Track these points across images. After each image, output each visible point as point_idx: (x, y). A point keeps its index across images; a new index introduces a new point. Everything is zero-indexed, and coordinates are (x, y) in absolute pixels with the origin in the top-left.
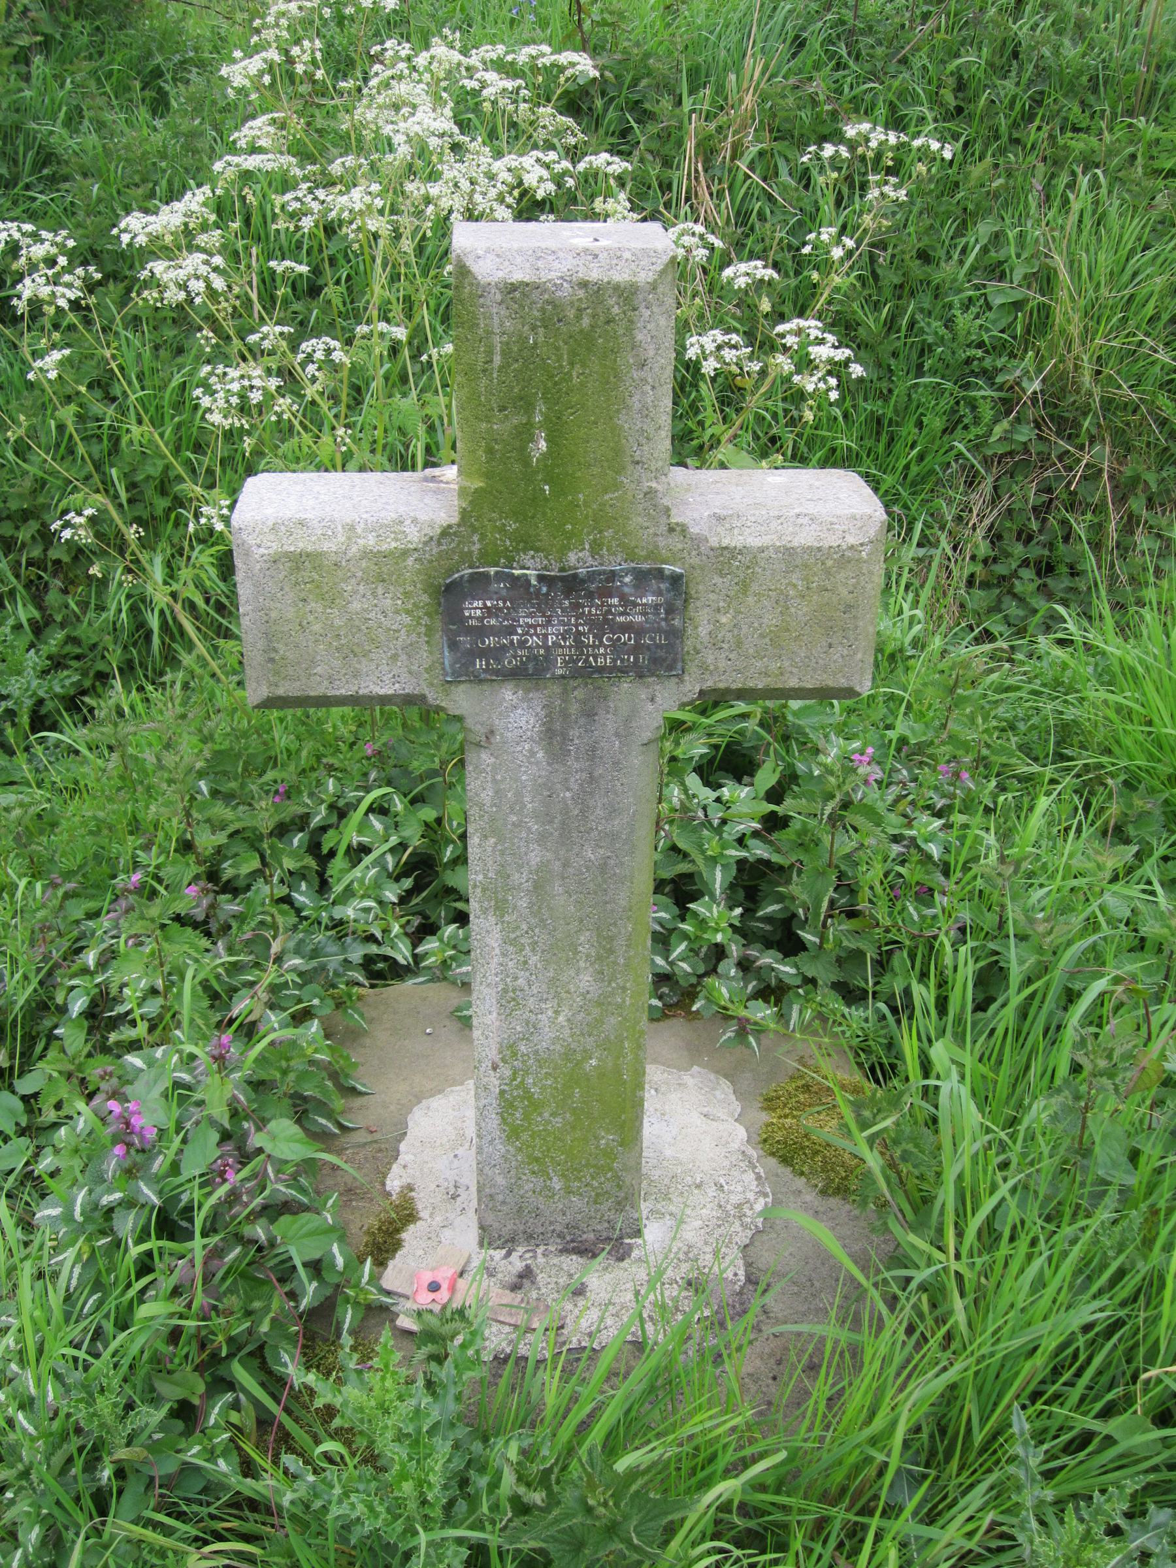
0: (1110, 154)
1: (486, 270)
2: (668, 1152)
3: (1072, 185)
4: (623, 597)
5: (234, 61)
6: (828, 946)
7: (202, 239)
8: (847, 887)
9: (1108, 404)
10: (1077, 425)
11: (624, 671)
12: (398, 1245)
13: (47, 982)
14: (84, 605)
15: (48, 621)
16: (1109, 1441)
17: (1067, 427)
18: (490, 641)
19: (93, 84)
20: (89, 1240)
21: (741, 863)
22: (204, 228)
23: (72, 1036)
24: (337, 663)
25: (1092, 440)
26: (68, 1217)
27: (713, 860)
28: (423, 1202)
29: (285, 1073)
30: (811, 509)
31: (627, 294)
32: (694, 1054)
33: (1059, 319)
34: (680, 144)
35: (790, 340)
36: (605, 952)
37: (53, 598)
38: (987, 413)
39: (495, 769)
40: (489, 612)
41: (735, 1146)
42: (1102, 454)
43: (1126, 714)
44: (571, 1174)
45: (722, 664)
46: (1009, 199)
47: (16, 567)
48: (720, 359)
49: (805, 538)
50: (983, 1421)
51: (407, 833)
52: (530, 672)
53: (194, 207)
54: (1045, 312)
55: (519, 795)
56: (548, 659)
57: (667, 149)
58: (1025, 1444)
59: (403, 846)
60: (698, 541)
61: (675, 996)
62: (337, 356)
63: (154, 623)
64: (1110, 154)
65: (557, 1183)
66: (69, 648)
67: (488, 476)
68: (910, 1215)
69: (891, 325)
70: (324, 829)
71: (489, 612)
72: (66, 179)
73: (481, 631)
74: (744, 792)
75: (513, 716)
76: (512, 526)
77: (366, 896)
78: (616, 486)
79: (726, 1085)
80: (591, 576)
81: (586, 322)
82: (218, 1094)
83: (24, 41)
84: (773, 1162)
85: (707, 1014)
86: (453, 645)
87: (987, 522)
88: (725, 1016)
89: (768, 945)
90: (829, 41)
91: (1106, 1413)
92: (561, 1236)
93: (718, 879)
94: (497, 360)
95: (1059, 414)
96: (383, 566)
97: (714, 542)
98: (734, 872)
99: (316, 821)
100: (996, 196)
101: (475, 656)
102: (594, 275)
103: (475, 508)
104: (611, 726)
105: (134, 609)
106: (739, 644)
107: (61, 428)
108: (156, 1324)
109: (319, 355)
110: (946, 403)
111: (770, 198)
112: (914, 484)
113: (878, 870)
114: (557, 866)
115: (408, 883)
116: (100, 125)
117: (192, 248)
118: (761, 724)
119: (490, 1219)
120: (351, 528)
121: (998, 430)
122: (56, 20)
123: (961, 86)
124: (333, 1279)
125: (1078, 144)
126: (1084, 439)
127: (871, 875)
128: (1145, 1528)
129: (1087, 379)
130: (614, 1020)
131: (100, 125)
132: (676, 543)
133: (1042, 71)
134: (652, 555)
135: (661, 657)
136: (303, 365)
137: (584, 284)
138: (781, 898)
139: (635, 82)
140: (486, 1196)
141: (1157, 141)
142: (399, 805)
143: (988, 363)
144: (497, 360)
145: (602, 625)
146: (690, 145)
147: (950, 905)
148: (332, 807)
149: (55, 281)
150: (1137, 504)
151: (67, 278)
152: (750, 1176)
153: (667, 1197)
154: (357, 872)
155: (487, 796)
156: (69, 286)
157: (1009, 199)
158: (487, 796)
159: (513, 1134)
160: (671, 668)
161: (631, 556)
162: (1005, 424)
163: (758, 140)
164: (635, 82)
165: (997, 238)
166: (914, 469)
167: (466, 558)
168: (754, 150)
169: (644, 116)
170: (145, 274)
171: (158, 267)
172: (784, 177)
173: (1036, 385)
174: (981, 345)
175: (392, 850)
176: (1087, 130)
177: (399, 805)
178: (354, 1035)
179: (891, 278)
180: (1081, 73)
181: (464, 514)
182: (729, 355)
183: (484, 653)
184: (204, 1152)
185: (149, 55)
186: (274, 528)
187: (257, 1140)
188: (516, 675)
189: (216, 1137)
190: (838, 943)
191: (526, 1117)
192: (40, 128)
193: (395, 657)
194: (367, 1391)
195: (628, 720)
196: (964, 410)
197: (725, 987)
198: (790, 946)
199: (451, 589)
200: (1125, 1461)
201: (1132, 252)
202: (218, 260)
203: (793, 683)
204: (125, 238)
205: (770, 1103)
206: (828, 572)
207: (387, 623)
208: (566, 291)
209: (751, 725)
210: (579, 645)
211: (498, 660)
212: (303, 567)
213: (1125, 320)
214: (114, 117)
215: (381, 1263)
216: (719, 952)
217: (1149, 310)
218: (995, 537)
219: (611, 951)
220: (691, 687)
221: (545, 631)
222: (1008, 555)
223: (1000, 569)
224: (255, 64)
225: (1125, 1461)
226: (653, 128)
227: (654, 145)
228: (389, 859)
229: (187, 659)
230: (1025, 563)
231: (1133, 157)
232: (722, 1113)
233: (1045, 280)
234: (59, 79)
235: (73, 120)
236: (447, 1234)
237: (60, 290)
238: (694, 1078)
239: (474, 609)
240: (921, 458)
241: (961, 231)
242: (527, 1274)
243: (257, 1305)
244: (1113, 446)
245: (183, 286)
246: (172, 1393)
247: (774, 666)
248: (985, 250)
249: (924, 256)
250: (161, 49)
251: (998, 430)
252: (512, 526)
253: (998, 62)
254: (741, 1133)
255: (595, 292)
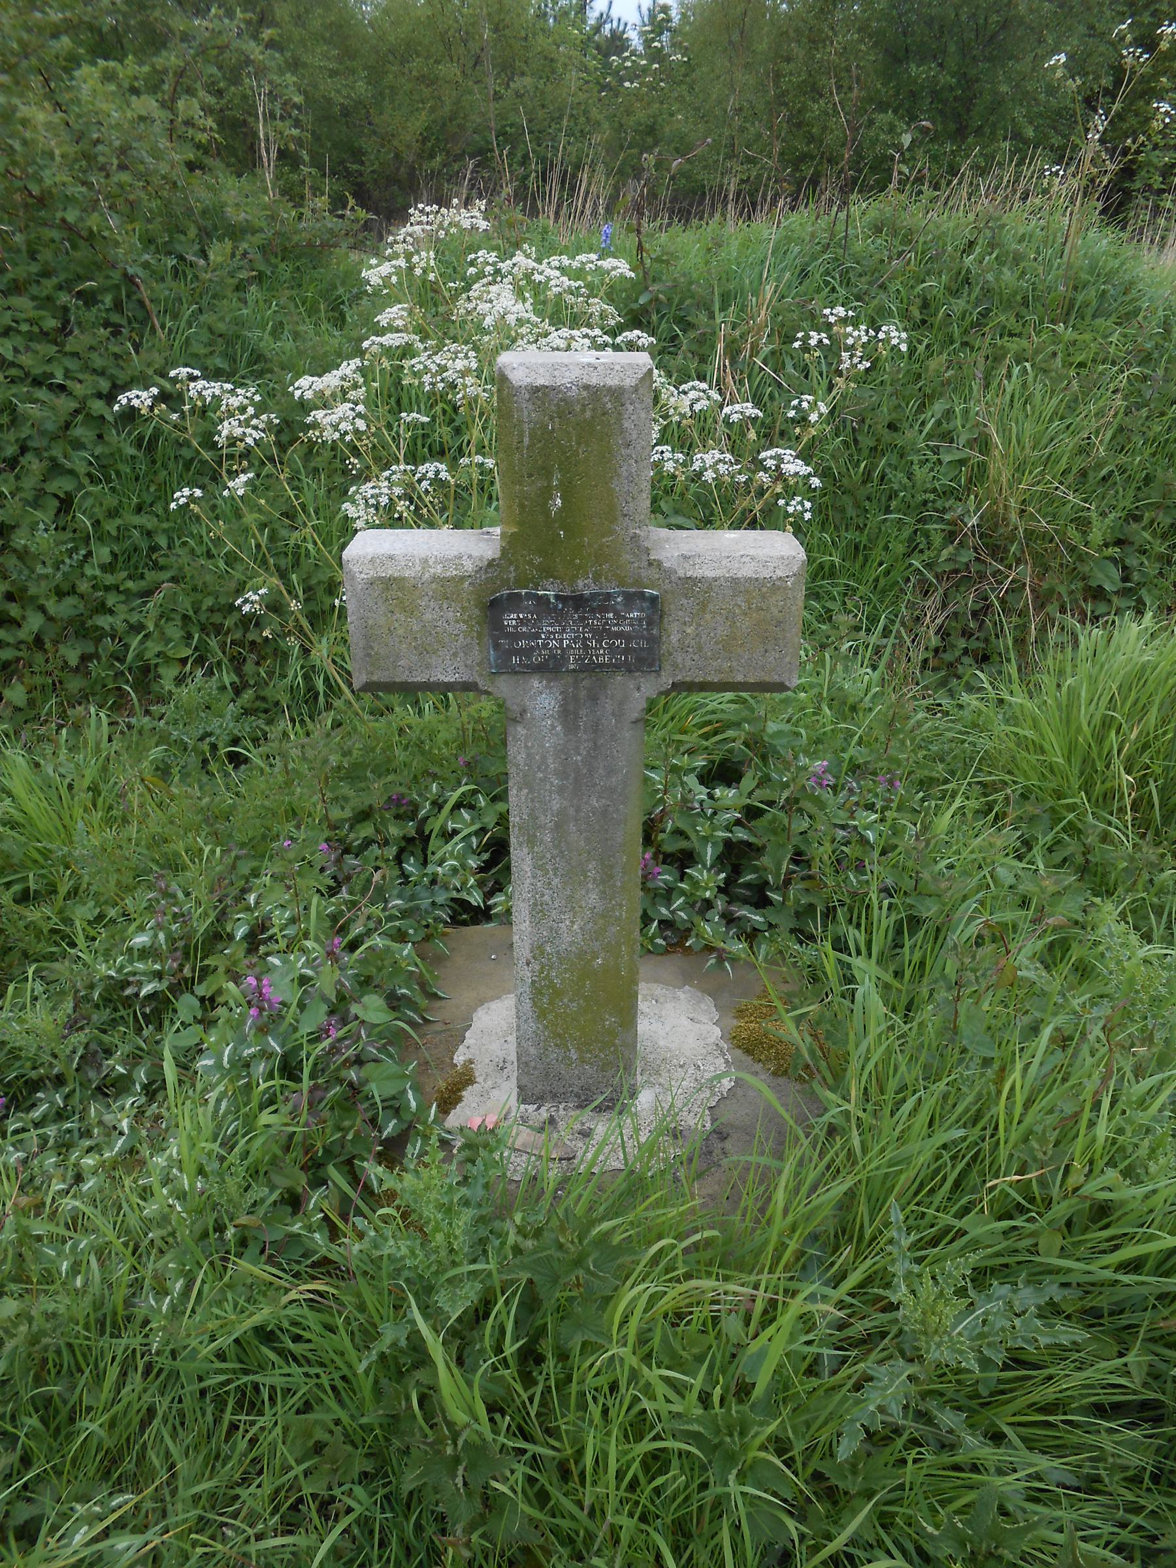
0: (1037, 352)
1: (519, 377)
2: (662, 1043)
3: (1009, 376)
4: (616, 613)
5: (371, 267)
6: (789, 904)
7: (352, 395)
8: (799, 858)
9: (1029, 534)
10: (1006, 550)
11: (617, 667)
12: (459, 1099)
13: (222, 916)
14: (270, 674)
15: (246, 685)
16: (962, 1233)
17: (998, 551)
18: (522, 643)
19: (292, 306)
20: (231, 1081)
21: (728, 843)
22: (356, 386)
23: (235, 950)
24: (415, 658)
25: (1019, 561)
26: (219, 1065)
27: (705, 839)
28: (479, 1071)
29: (380, 970)
30: (752, 552)
31: (617, 393)
32: (687, 978)
33: (992, 472)
34: (713, 347)
35: (770, 463)
36: (606, 878)
37: (249, 668)
38: (937, 540)
39: (527, 738)
40: (522, 622)
41: (711, 1040)
42: (1026, 572)
43: (1021, 742)
44: (585, 1055)
45: (689, 663)
46: (959, 386)
47: (223, 646)
48: (716, 471)
49: (747, 571)
50: (872, 1221)
51: (486, 820)
52: (550, 668)
53: (348, 372)
54: (982, 466)
55: (544, 758)
56: (564, 658)
57: (704, 350)
58: (899, 1229)
59: (483, 830)
60: (670, 572)
61: (675, 938)
62: (443, 475)
63: (320, 686)
64: (1037, 352)
65: (574, 1055)
66: (258, 704)
67: (521, 524)
68: (830, 1080)
69: (867, 477)
70: (426, 819)
71: (522, 622)
72: (271, 371)
73: (516, 636)
74: (732, 792)
75: (542, 699)
76: (537, 560)
77: (453, 862)
78: (611, 532)
79: (709, 1000)
80: (593, 596)
81: (588, 414)
82: (328, 980)
83: (243, 275)
84: (739, 1052)
85: (697, 948)
86: (496, 646)
87: (939, 621)
88: (709, 949)
89: (745, 901)
90: (827, 273)
91: (960, 1215)
92: (578, 1096)
93: (709, 853)
94: (526, 440)
95: (992, 539)
96: (447, 588)
97: (681, 573)
98: (721, 848)
99: (422, 813)
100: (949, 382)
101: (513, 657)
102: (594, 381)
103: (511, 545)
104: (609, 708)
105: (306, 677)
106: (700, 649)
107: (258, 546)
108: (272, 1131)
109: (431, 475)
110: (906, 533)
111: (780, 385)
112: (884, 591)
113: (828, 847)
114: (572, 811)
115: (486, 856)
116: (296, 336)
117: (345, 400)
118: (745, 744)
119: (524, 1081)
120: (425, 561)
121: (945, 553)
122: (267, 261)
123: (925, 305)
124: (408, 1117)
125: (1013, 345)
126: (1011, 559)
127: (822, 852)
128: (989, 1298)
129: (1014, 517)
130: (615, 929)
131: (296, 336)
132: (654, 573)
133: (987, 292)
134: (638, 582)
135: (644, 658)
136: (420, 481)
137: (586, 387)
138: (756, 870)
139: (681, 302)
140: (523, 1064)
141: (1074, 343)
142: (482, 801)
143: (939, 504)
144: (526, 440)
145: (601, 633)
146: (720, 347)
147: (878, 872)
148: (434, 803)
149: (246, 423)
150: (1052, 608)
151: (254, 422)
152: (720, 1061)
153: (658, 1073)
154: (449, 847)
155: (521, 758)
156: (255, 428)
157: (959, 386)
158: (521, 758)
159: (541, 1014)
160: (651, 665)
161: (622, 584)
162: (951, 548)
163: (769, 342)
164: (681, 302)
165: (949, 414)
166: (882, 582)
167: (505, 583)
168: (766, 350)
169: (687, 326)
170: (309, 420)
171: (319, 414)
172: (790, 369)
173: (974, 521)
174: (934, 490)
175: (476, 833)
176: (1020, 335)
177: (482, 801)
178: (439, 960)
179: (867, 442)
180: (1016, 293)
181: (503, 550)
182: (722, 468)
183: (519, 652)
184: (318, 1015)
185: (335, 288)
186: (372, 561)
187: (355, 1009)
188: (540, 669)
189: (324, 1008)
190: (797, 901)
191: (551, 1003)
192: (253, 335)
193: (455, 655)
194: (422, 1181)
195: (621, 703)
196: (920, 539)
197: (709, 929)
198: (761, 902)
199: (493, 602)
200: (974, 1245)
201: (1051, 420)
202: (361, 408)
203: (740, 678)
204: (298, 393)
205: (741, 1013)
206: (763, 597)
207: (449, 629)
208: (574, 392)
209: (738, 745)
210: (586, 647)
211: (529, 658)
212: (392, 587)
213: (1042, 473)
214: (307, 328)
215: (446, 1112)
216: (708, 904)
217: (1063, 465)
218: (944, 633)
219: (611, 877)
220: (666, 680)
221: (559, 637)
222: (953, 646)
223: (948, 657)
224: (386, 268)
225: (974, 1245)
226: (692, 334)
227: (694, 347)
228: (474, 840)
229: (337, 703)
230: (966, 651)
231: (1055, 354)
232: (704, 1019)
233: (983, 443)
234: (268, 302)
235: (276, 333)
236: (495, 1092)
237: (249, 431)
238: (684, 994)
239: (511, 620)
240: (887, 573)
241: (922, 408)
242: (552, 1121)
243: (347, 1123)
244: (1034, 565)
245: (336, 427)
246: (282, 1182)
247: (727, 665)
248: (939, 423)
249: (892, 427)
250: (343, 284)
251: (945, 553)
252: (537, 560)
253: (954, 287)
254: (717, 1032)
255: (594, 393)
